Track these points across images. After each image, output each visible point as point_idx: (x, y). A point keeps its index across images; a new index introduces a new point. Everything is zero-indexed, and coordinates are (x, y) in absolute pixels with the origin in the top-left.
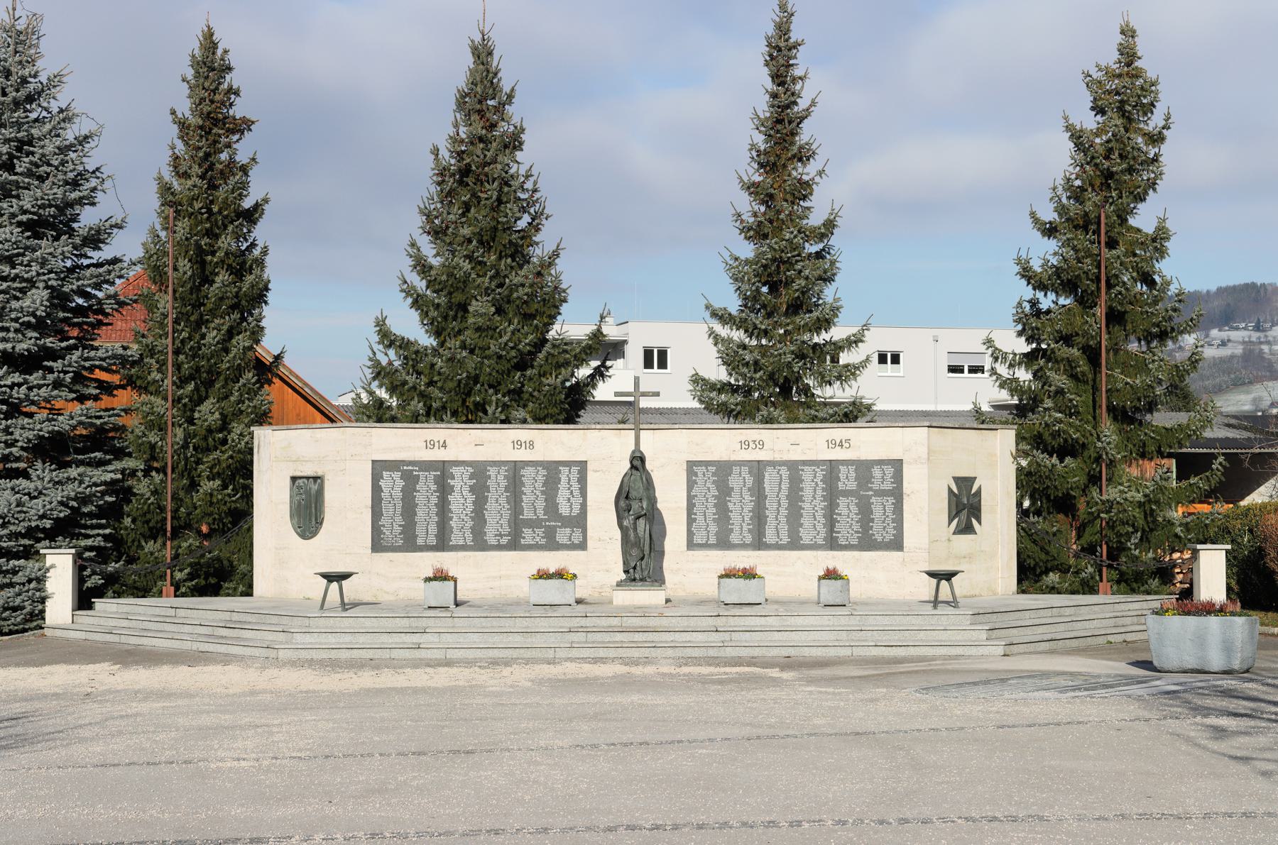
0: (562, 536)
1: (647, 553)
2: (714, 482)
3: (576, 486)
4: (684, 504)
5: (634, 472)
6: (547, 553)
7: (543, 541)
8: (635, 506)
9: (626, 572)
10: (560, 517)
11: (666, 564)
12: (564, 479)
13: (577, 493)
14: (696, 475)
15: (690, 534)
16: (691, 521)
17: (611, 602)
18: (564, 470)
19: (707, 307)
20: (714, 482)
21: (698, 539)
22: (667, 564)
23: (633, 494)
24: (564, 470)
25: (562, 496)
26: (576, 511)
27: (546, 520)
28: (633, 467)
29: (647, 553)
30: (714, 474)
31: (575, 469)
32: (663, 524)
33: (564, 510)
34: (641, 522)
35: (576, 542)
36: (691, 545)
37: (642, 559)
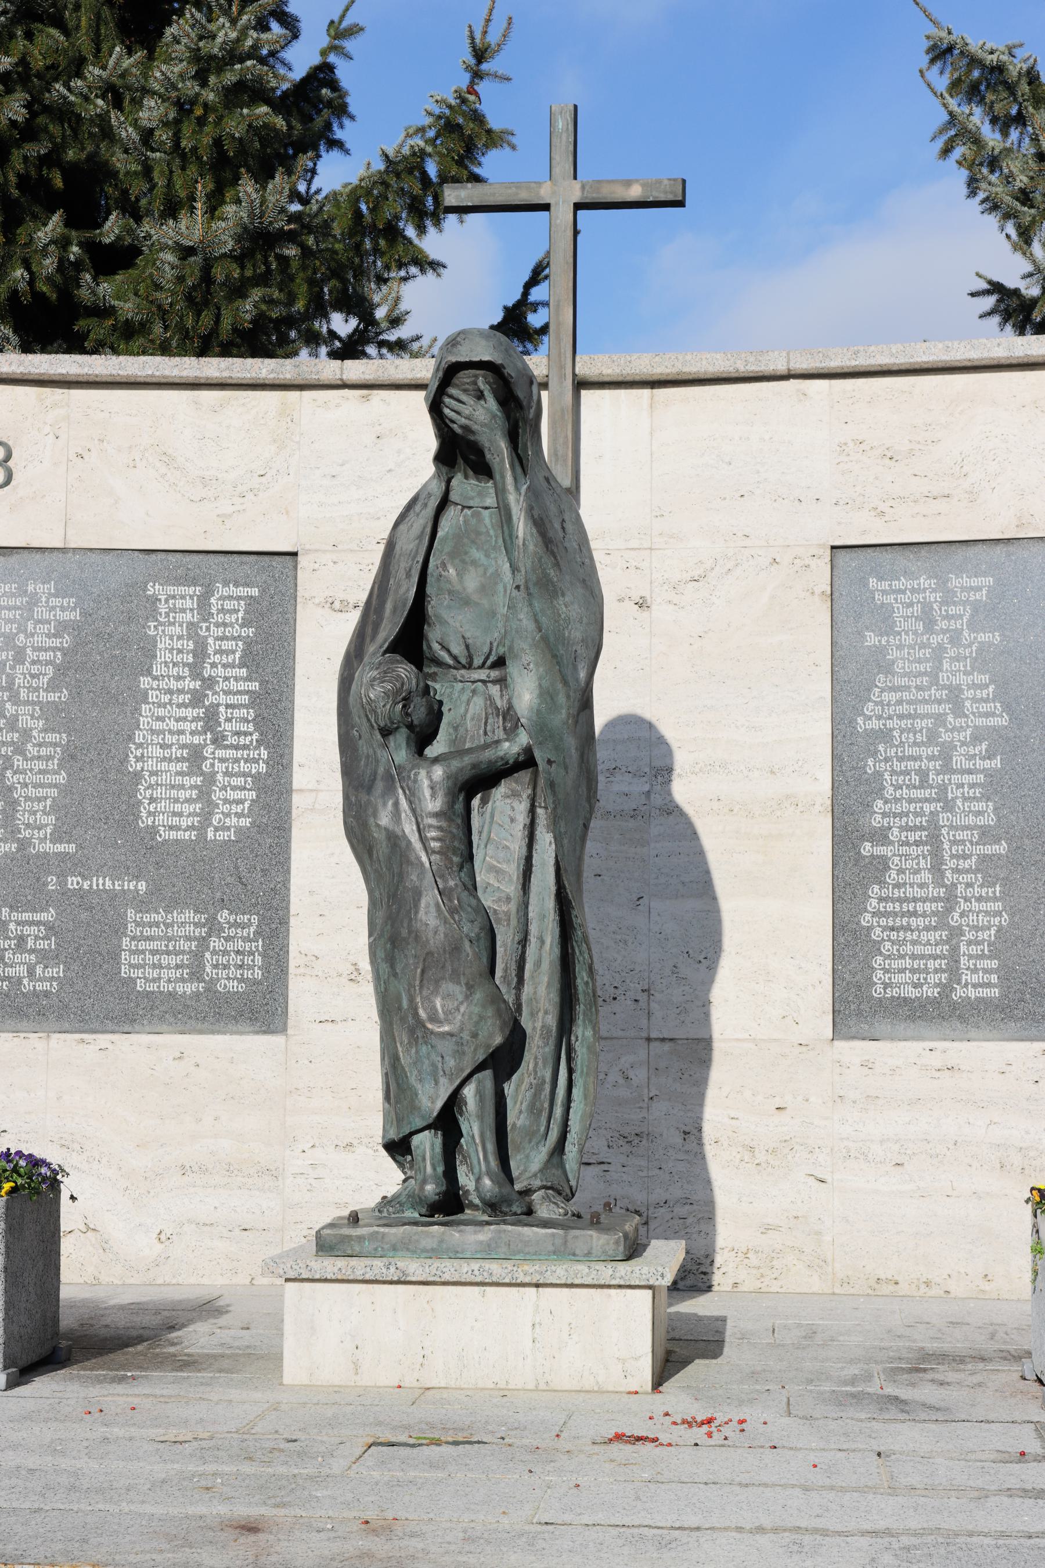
0: (155, 949)
1: (539, 1016)
2: (982, 660)
3: (233, 687)
4: (818, 782)
5: (464, 486)
6: (64, 1046)
7: (49, 978)
8: (466, 708)
9: (398, 1148)
10: (147, 851)
11: (717, 1115)
12: (170, 644)
13: (237, 720)
14: (885, 623)
15: (850, 943)
16: (854, 869)
17: (260, 1360)
18: (176, 601)
19: (940, 53)
20: (982, 660)
21: (893, 976)
22: (727, 1109)
23: (451, 628)
24: (176, 601)
25: (161, 731)
26: (233, 814)
27: (65, 865)
28: (457, 451)
29: (539, 1016)
30: (983, 615)
31: (231, 599)
32: (701, 886)
33: (168, 808)
34: (503, 814)
35: (229, 984)
36: (858, 1007)
37: (504, 1060)
